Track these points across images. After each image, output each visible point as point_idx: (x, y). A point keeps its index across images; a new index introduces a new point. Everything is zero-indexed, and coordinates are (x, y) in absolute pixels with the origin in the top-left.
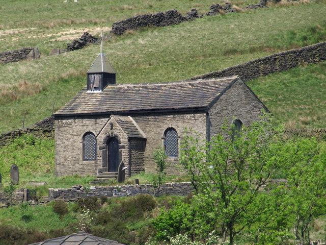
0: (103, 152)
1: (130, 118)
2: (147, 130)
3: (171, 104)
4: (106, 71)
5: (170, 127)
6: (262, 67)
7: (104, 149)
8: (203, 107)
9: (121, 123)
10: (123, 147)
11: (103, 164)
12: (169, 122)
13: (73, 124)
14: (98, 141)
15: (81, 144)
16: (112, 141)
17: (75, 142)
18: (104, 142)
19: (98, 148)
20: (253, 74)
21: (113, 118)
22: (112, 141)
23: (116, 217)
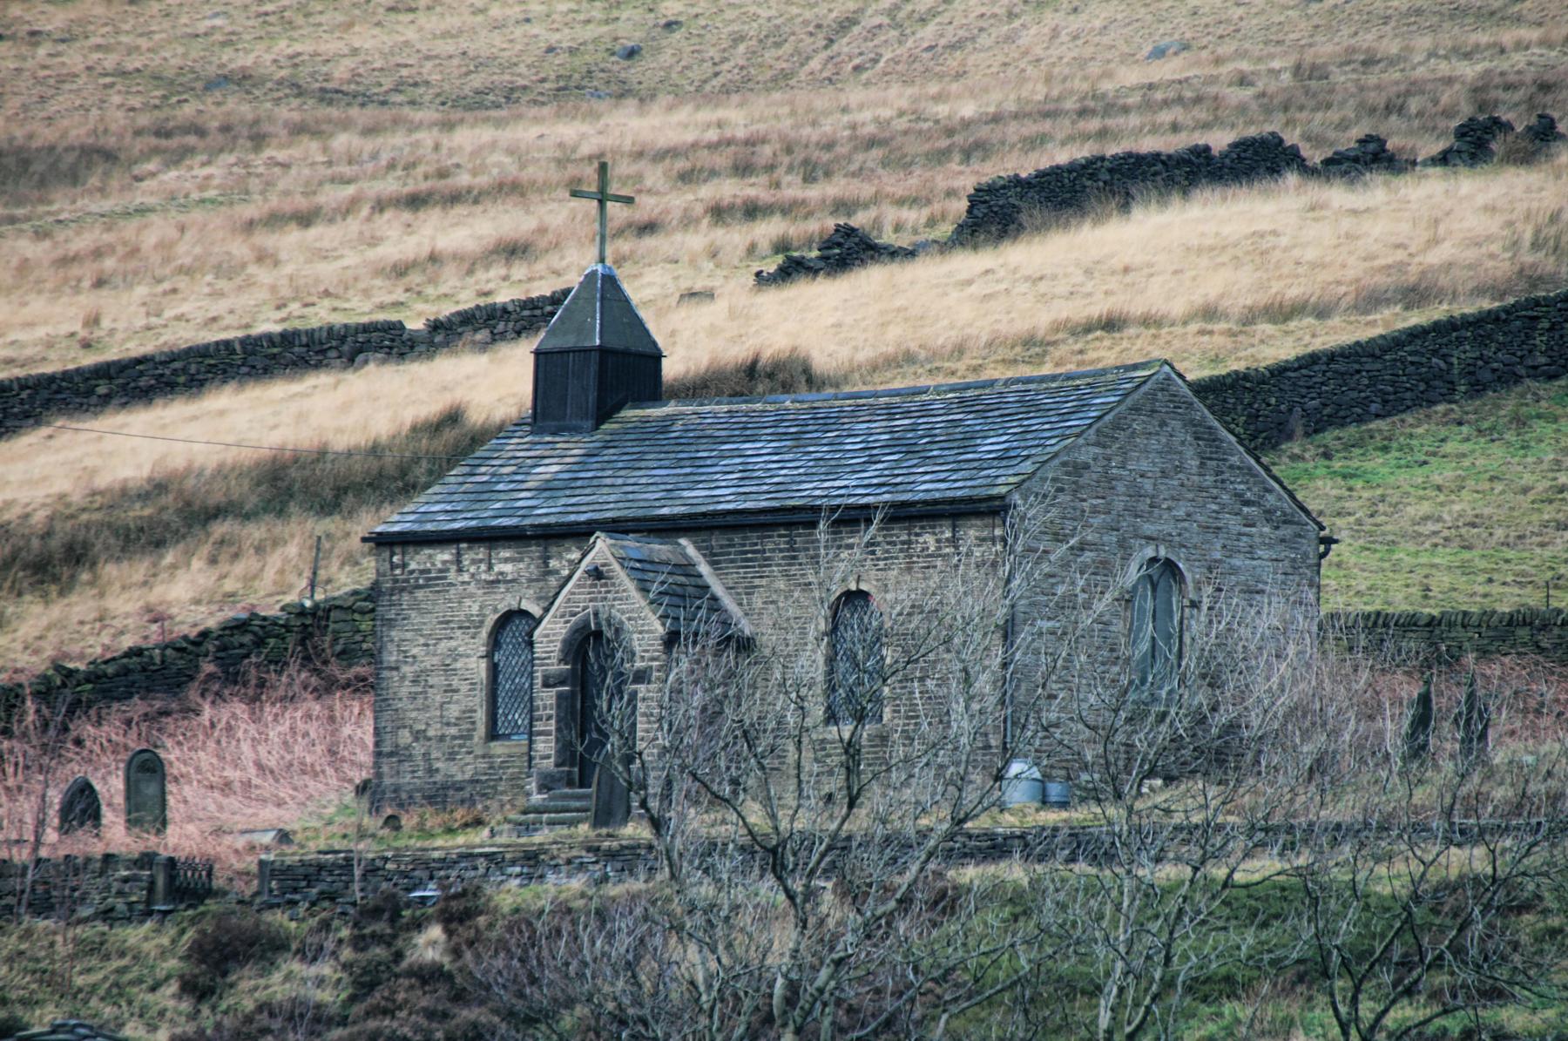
0: (560, 696)
1: (688, 546)
2: (757, 601)
3: (252, 346)
4: (616, 343)
5: (853, 587)
6: (1468, 352)
7: (562, 683)
8: (991, 498)
9: (642, 570)
10: (641, 677)
11: (559, 752)
12: (844, 564)
13: (452, 575)
14: (538, 648)
15: (483, 664)
16: (590, 645)
17: (455, 655)
18: (566, 655)
19: (539, 681)
20: (1422, 387)
21: (602, 547)
22: (590, 645)
23: (20, 821)
